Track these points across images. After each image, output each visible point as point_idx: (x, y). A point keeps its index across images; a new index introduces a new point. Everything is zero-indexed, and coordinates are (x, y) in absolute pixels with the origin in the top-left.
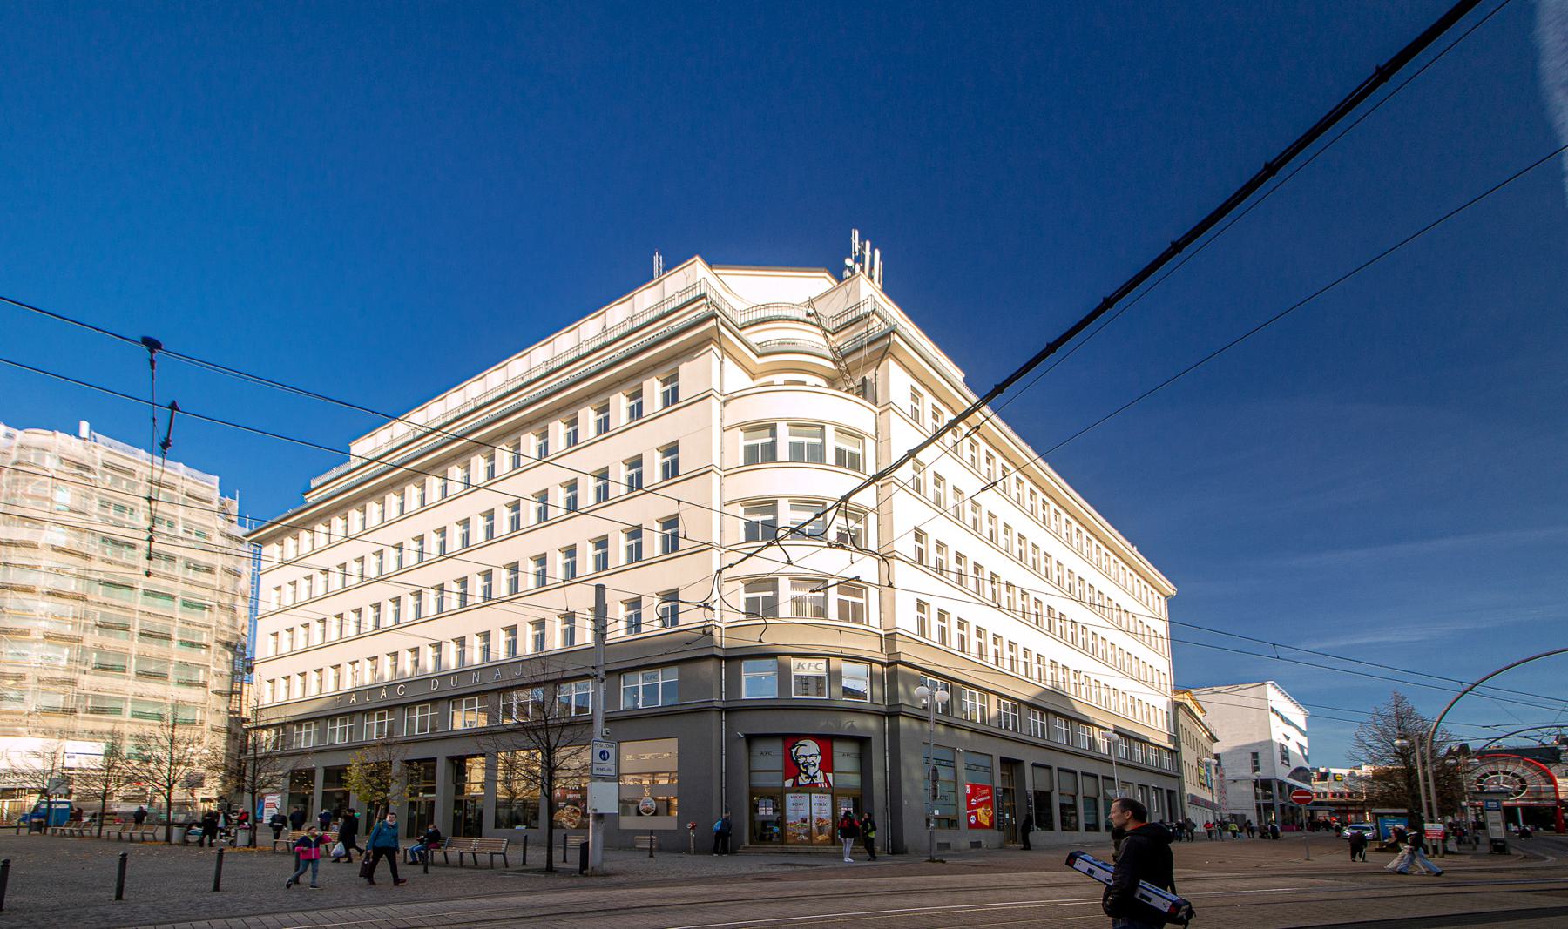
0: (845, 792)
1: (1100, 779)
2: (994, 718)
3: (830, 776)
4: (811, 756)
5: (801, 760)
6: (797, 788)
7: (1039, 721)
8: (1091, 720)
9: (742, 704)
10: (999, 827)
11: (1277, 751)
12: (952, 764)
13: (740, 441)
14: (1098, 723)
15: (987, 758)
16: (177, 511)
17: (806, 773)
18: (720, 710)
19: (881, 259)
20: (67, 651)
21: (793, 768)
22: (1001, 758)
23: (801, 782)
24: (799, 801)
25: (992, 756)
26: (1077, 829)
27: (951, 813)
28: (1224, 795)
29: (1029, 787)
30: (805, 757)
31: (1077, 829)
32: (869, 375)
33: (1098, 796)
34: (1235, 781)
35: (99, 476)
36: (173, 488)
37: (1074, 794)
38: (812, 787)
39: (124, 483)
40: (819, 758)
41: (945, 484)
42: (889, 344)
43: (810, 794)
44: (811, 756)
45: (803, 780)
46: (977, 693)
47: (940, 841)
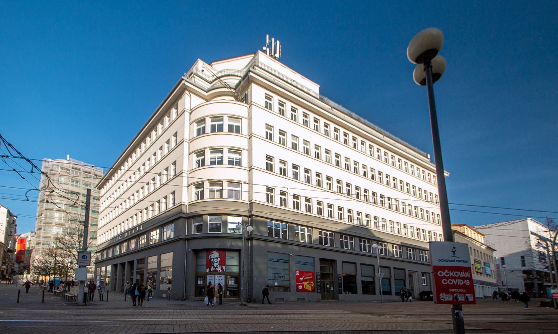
0: (232, 275)
1: (359, 266)
2: (316, 240)
3: (224, 267)
4: (215, 258)
5: (212, 260)
6: (211, 273)
7: (349, 241)
8: (384, 240)
9: (192, 236)
10: (317, 291)
11: (535, 255)
12: (287, 261)
13: (195, 127)
14: (388, 241)
15: (312, 259)
16: (91, 181)
17: (213, 266)
18: (185, 240)
19: (280, 44)
20: (62, 228)
21: (209, 264)
22: (320, 258)
23: (212, 270)
24: (221, 278)
25: (314, 257)
26: (374, 293)
27: (286, 284)
28: (500, 278)
29: (340, 272)
30: (213, 259)
31: (374, 293)
32: (246, 92)
33: (406, 279)
34: (512, 271)
35: (71, 172)
36: (90, 173)
37: (389, 278)
38: (216, 272)
39: (79, 173)
40: (219, 259)
41: (357, 140)
42: (248, 78)
43: (215, 275)
44: (215, 258)
45: (212, 269)
46: (306, 229)
47: (277, 297)
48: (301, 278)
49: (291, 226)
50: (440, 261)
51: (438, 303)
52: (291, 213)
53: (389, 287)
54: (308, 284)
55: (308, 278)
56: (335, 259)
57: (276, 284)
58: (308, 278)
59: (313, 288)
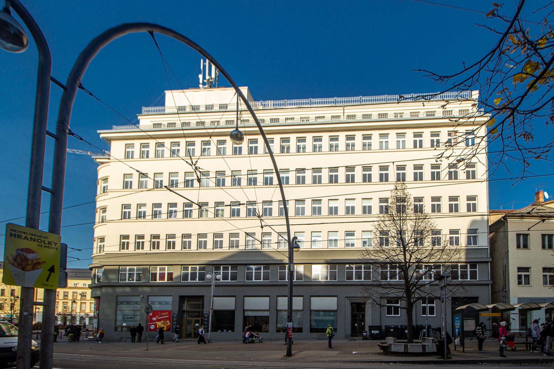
48: (406, 331)
49: (144, 271)
50: (109, 165)
51: (138, 342)
52: (136, 254)
53: (73, 306)
54: (162, 323)
55: (164, 317)
56: (55, 270)
57: (124, 324)
58: (164, 317)
59: (169, 328)
